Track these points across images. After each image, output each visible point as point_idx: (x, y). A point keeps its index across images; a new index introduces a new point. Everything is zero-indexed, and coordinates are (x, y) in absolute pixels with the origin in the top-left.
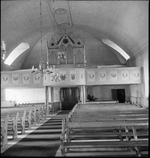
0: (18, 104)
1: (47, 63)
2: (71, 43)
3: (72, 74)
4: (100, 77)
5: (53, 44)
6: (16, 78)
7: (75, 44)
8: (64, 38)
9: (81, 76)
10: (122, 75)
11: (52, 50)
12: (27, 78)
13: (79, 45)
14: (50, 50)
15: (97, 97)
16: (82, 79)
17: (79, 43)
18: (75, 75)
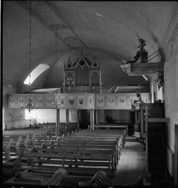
0: (39, 124)
1: (64, 85)
2: (88, 65)
3: (80, 98)
4: (108, 102)
5: (69, 66)
6: (122, 100)
7: (92, 65)
8: (80, 59)
9: (90, 100)
10: (47, 101)
11: (68, 72)
12: (101, 101)
13: (95, 67)
14: (66, 71)
15: (116, 119)
16: (91, 103)
17: (95, 65)
18: (83, 99)
